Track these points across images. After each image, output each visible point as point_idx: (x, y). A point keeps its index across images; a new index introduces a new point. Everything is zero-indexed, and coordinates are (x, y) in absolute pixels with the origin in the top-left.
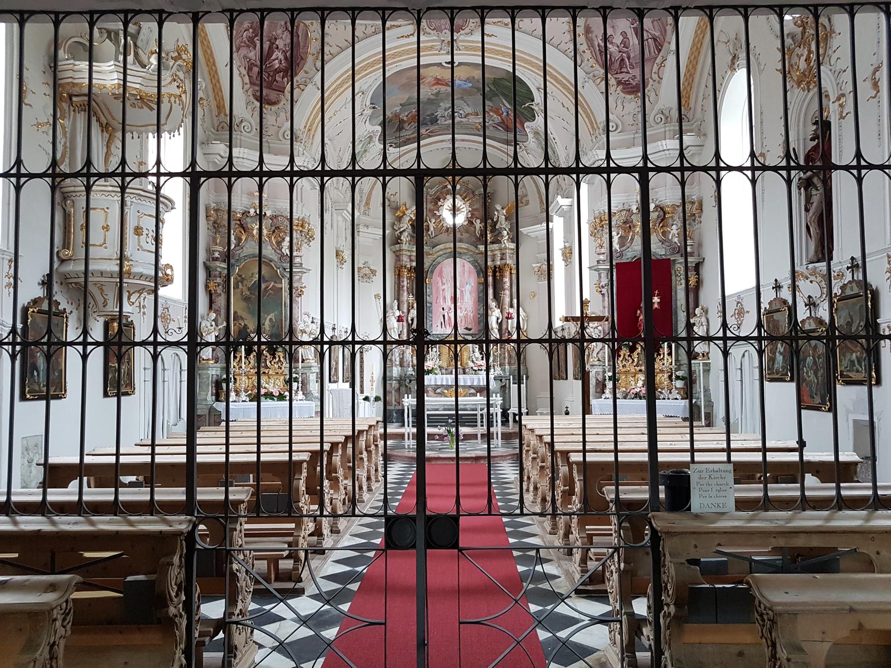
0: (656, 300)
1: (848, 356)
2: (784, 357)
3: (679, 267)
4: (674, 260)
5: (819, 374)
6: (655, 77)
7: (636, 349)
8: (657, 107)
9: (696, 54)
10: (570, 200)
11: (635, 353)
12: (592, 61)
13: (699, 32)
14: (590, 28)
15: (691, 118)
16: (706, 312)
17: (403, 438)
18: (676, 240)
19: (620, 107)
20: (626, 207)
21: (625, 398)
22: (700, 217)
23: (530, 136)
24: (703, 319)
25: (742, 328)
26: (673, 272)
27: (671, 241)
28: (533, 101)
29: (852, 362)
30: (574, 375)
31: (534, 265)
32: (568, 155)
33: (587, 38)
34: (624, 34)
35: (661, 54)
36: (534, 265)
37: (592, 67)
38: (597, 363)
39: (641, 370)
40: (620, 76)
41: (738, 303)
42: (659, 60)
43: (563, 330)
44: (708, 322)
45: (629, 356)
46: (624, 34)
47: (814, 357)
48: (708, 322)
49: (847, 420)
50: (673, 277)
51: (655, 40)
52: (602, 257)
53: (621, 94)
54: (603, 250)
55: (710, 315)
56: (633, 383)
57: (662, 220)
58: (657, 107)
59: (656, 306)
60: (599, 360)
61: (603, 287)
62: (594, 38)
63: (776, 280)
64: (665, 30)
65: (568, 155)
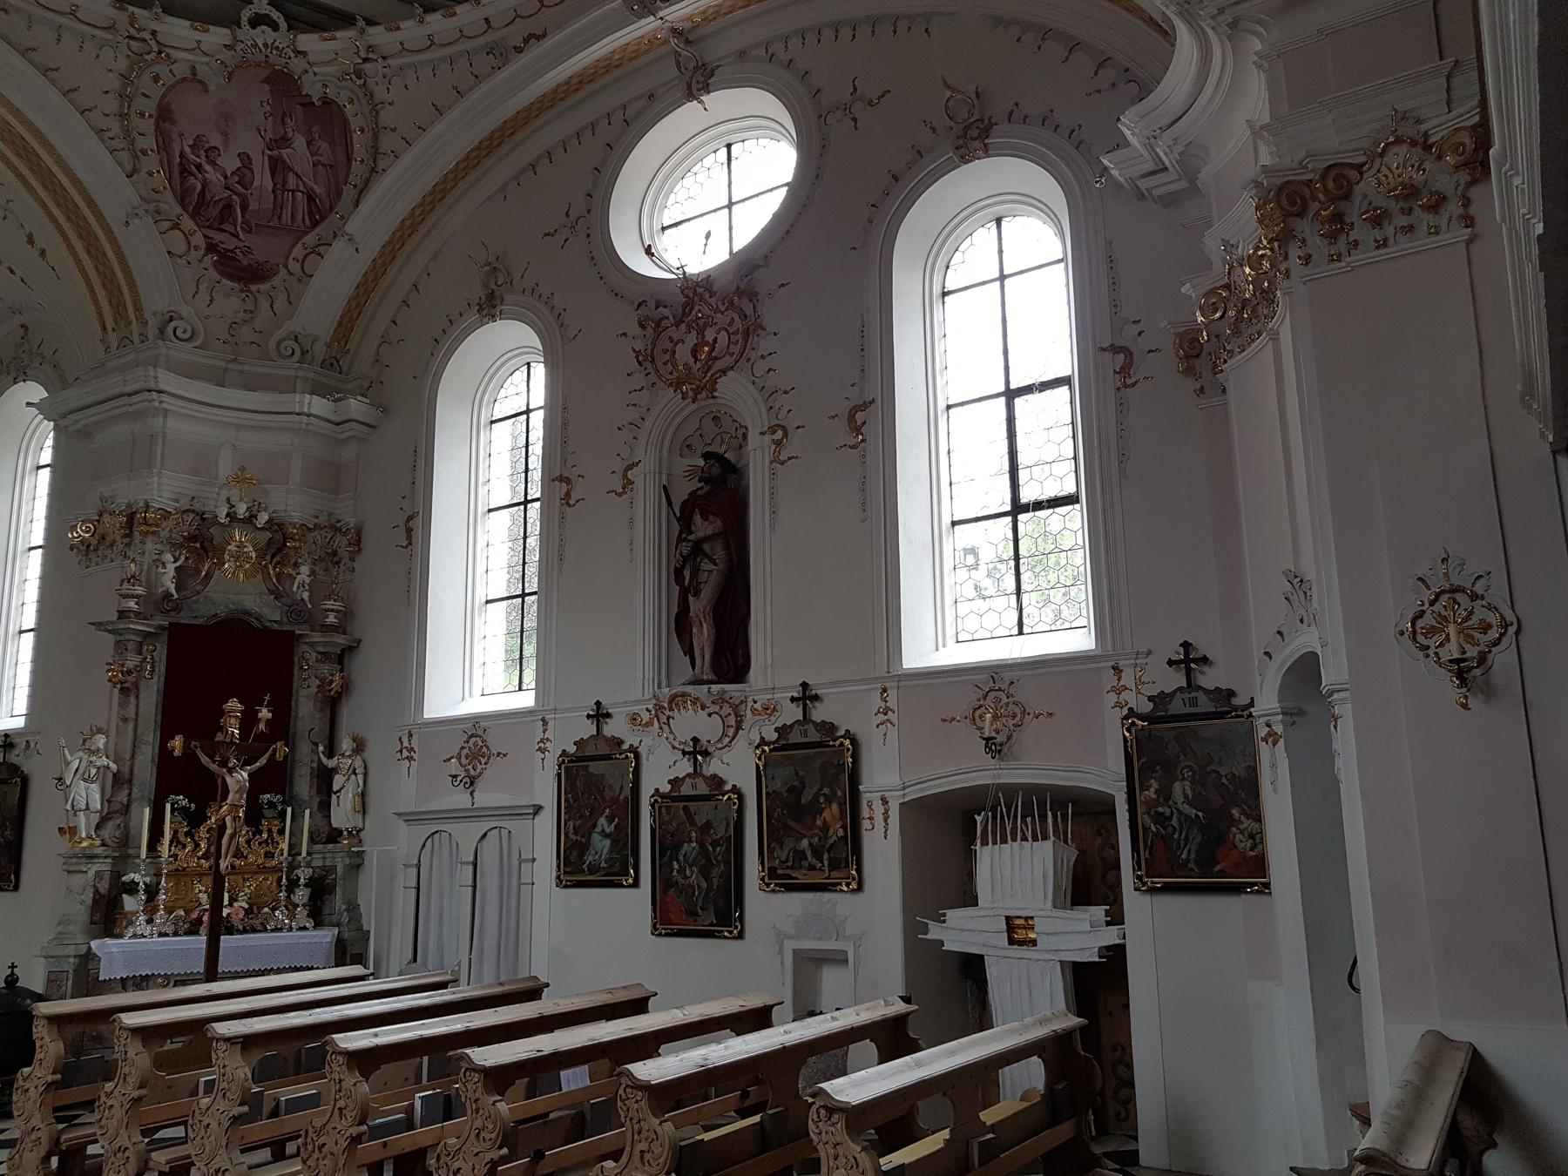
1: (790, 843)
2: (613, 842)
3: (306, 655)
4: (301, 636)
5: (715, 873)
7: (206, 818)
11: (203, 832)
12: (160, 178)
13: (408, 223)
14: (170, 111)
15: (345, 369)
16: (360, 746)
17: (194, 1093)
18: (306, 595)
19: (203, 296)
20: (197, 507)
24: (358, 763)
25: (479, 784)
29: (801, 855)
33: (157, 127)
34: (245, 158)
35: (318, 230)
38: (100, 851)
40: (218, 237)
42: (310, 239)
45: (187, 834)
46: (245, 158)
47: (701, 843)
49: (781, 952)
51: (311, 198)
52: (132, 604)
54: (140, 590)
57: (279, 550)
59: (262, 726)
60: (103, 845)
61: (129, 672)
62: (175, 136)
63: (598, 704)
64: (339, 194)
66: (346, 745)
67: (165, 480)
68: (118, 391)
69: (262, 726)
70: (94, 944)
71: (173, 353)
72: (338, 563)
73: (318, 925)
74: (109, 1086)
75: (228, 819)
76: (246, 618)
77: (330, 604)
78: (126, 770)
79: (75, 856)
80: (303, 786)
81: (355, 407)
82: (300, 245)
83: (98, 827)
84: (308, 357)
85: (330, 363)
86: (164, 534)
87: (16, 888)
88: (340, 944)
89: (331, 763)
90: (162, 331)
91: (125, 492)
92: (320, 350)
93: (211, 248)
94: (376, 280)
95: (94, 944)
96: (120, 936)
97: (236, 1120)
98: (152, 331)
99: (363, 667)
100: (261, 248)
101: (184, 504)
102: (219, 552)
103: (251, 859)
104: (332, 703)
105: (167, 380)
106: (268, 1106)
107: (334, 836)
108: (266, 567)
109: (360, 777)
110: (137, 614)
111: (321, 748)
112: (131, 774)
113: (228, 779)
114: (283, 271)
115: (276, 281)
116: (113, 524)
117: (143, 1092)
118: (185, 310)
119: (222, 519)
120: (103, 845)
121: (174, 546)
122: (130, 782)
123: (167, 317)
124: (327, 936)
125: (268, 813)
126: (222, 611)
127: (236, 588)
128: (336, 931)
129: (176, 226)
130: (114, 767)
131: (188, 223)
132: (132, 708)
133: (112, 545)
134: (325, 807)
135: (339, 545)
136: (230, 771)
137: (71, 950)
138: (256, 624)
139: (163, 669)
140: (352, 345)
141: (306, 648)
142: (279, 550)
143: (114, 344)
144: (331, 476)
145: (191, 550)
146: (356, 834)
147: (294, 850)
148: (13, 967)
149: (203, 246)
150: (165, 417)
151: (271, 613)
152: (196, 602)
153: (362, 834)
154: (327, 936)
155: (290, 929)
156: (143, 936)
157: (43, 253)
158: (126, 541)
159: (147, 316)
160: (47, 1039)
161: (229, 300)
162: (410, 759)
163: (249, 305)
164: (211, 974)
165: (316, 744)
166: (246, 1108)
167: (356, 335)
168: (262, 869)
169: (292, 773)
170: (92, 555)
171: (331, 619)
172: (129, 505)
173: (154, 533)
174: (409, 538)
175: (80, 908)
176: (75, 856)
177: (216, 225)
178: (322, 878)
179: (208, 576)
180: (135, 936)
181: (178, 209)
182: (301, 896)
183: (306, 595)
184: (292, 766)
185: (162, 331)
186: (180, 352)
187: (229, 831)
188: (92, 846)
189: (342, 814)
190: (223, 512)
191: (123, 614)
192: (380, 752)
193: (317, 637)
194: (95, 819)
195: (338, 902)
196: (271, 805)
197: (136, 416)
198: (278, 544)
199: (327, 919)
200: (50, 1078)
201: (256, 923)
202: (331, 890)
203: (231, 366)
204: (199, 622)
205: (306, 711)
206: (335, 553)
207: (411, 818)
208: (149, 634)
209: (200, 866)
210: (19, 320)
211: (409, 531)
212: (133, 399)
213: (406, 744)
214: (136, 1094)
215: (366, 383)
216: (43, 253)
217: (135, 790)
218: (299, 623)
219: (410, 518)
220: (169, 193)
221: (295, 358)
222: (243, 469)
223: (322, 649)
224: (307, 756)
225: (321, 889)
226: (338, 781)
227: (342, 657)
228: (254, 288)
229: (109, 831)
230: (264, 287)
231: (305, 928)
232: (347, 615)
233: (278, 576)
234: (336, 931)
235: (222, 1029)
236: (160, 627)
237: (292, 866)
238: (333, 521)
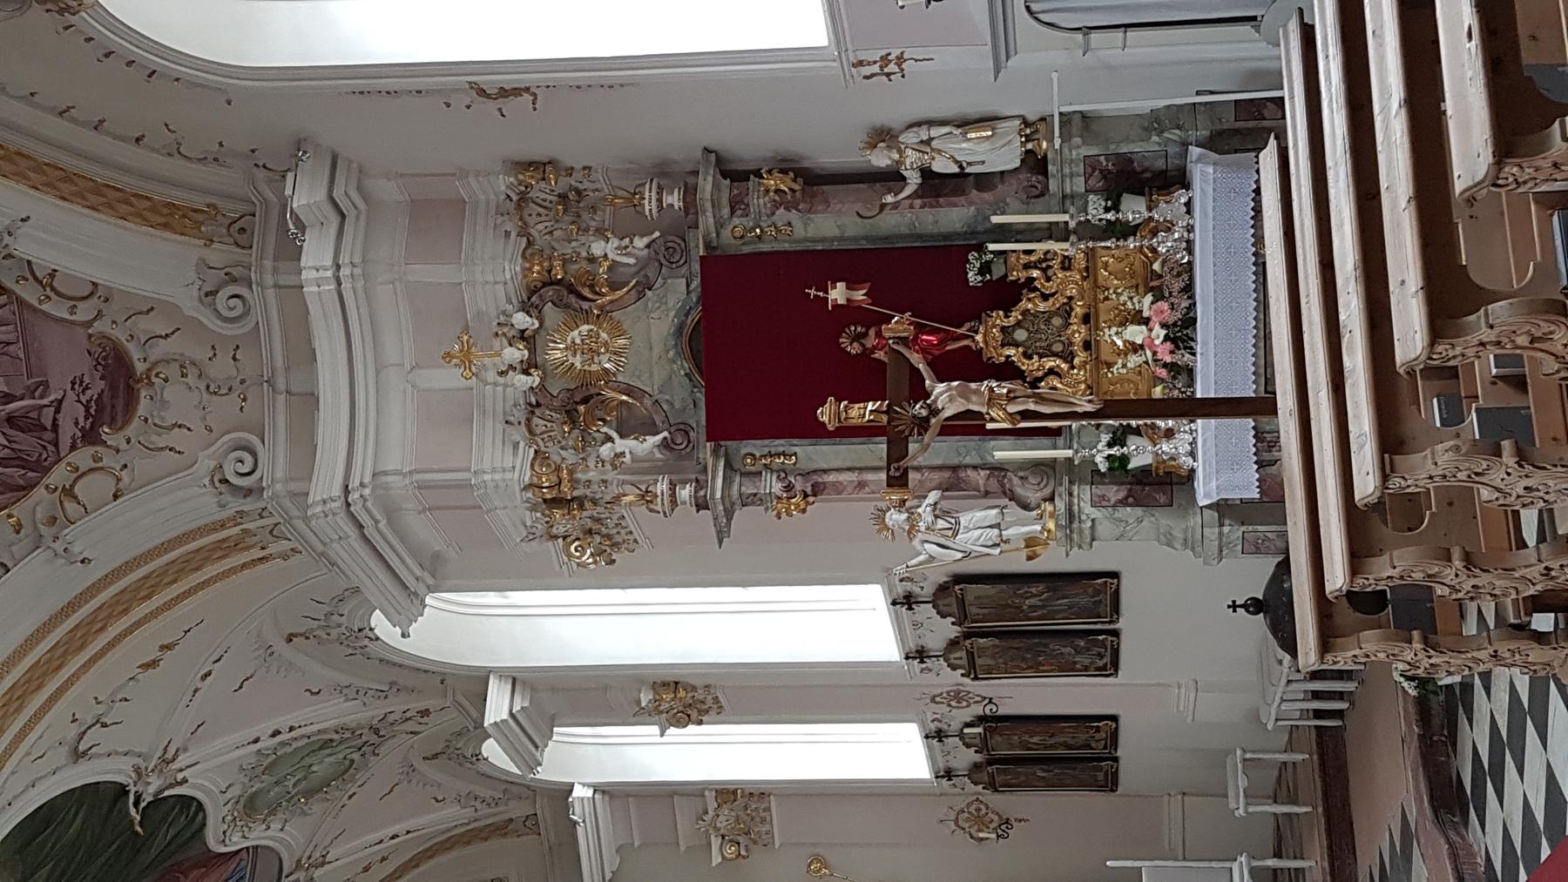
0: (838, 294)
3: (734, 234)
4: (707, 245)
6: (84, 312)
7: (1009, 362)
8: (190, 305)
9: (23, 163)
10: (493, 684)
11: (1025, 365)
15: (243, 208)
16: (883, 136)
18: (640, 242)
19: (176, 438)
20: (520, 415)
21: (1190, 372)
22: (570, 171)
23: (258, 836)
24: (909, 138)
26: (746, 249)
27: (642, 265)
28: (122, 790)
30: (1102, 671)
31: (716, 859)
32: (341, 689)
36: (716, 859)
37: (18, 528)
38: (1060, 504)
39: (1087, 346)
40: (67, 431)
41: (933, 700)
42: (29, 293)
43: (939, 735)
44: (919, 124)
48: (919, 124)
50: (765, 247)
52: (685, 493)
53: (130, 431)
54: (662, 487)
55: (893, 116)
56: (1134, 360)
57: (572, 290)
58: (190, 305)
59: (859, 295)
60: (1051, 499)
61: (789, 488)
65: (341, 689)
66: (881, 159)
67: (487, 466)
68: (358, 545)
69: (859, 295)
70: (1202, 502)
71: (279, 474)
72: (579, 192)
73: (1181, 180)
74: (1440, 590)
75: (1012, 409)
76: (687, 331)
77: (650, 206)
78: (937, 476)
79: (1069, 538)
80: (953, 217)
81: (305, 195)
82: (44, 307)
83: (1026, 507)
84: (236, 272)
85: (240, 232)
86: (570, 457)
87: (1115, 575)
88: (1220, 142)
89: (914, 179)
90: (249, 492)
91: (514, 514)
92: (220, 254)
93: (90, 436)
94: (70, 177)
95: (1202, 502)
96: (1192, 471)
97: (1522, 457)
98: (249, 505)
99: (747, 138)
100: (66, 365)
101: (519, 434)
102: (586, 380)
103: (1072, 291)
104: (813, 182)
105: (325, 485)
106: (1507, 398)
107: (1035, 164)
108: (601, 308)
109: (935, 132)
110: (699, 485)
111: (889, 199)
112: (941, 468)
113: (948, 413)
114: (98, 326)
115: (120, 335)
116: (562, 522)
117: (1456, 554)
118: (206, 464)
119: (535, 380)
120: (1051, 499)
121: (586, 442)
122: (955, 469)
123: (222, 488)
124: (1204, 172)
125: (998, 271)
126: (683, 367)
127: (645, 344)
128: (1195, 151)
129: (69, 492)
130: (933, 496)
131: (59, 475)
132: (844, 477)
133: (598, 520)
134: (985, 181)
135: (549, 193)
136: (934, 412)
137: (1212, 533)
138: (695, 315)
139: (781, 441)
140: (200, 201)
141: (726, 232)
142: (572, 290)
143: (285, 545)
144: (435, 215)
145: (592, 418)
146: (1031, 128)
147: (1058, 232)
148: (1234, 606)
149: (91, 450)
150: (385, 473)
151: (676, 294)
152: (671, 404)
153: (1031, 117)
154: (1204, 172)
155: (1190, 229)
156: (1193, 443)
157: (166, 647)
158: (587, 504)
159: (230, 512)
160: (1357, 652)
161: (172, 400)
162: (900, 60)
163: (173, 371)
164: (1263, 406)
165: (883, 206)
166: (1506, 445)
167: (179, 197)
168: (1089, 272)
169: (932, 236)
170: (618, 539)
171: (674, 199)
172: (534, 508)
173: (571, 473)
174: (517, 92)
175: (1143, 524)
176: (1069, 538)
177: (49, 436)
178: (1105, 174)
179: (629, 390)
180: (1193, 454)
181: (40, 492)
182: (1133, 209)
183: (640, 242)
184: (920, 237)
185: (249, 492)
186: (275, 465)
187: (1032, 407)
188: (1052, 515)
189: (996, 153)
190: (522, 381)
191: (701, 505)
192: (891, 104)
193: (707, 220)
194: (1013, 510)
195: (1147, 149)
196: (985, 269)
197: (391, 511)
198: (560, 290)
199: (1174, 162)
200: (1418, 646)
201: (1177, 285)
202: (1125, 161)
203: (281, 386)
204: (701, 397)
205: (830, 224)
206: (563, 197)
207: (1003, 47)
208: (729, 465)
209: (1083, 365)
210: (280, 646)
211: (504, 93)
212: (365, 519)
213: (876, 69)
214: (1458, 564)
215: (261, 174)
216: (166, 647)
217: (968, 460)
218: (686, 251)
219: (482, 92)
220: (15, 510)
221: (243, 291)
222: (448, 356)
223: (726, 211)
224: (900, 217)
225: (1125, 178)
226: (942, 166)
227: (736, 174)
228: (140, 367)
229: (1031, 494)
230: (135, 353)
231: (1188, 204)
232: (663, 173)
233: (614, 287)
234: (1195, 151)
235: (1366, 485)
236: (715, 452)
237: (1088, 231)
238: (511, 206)
